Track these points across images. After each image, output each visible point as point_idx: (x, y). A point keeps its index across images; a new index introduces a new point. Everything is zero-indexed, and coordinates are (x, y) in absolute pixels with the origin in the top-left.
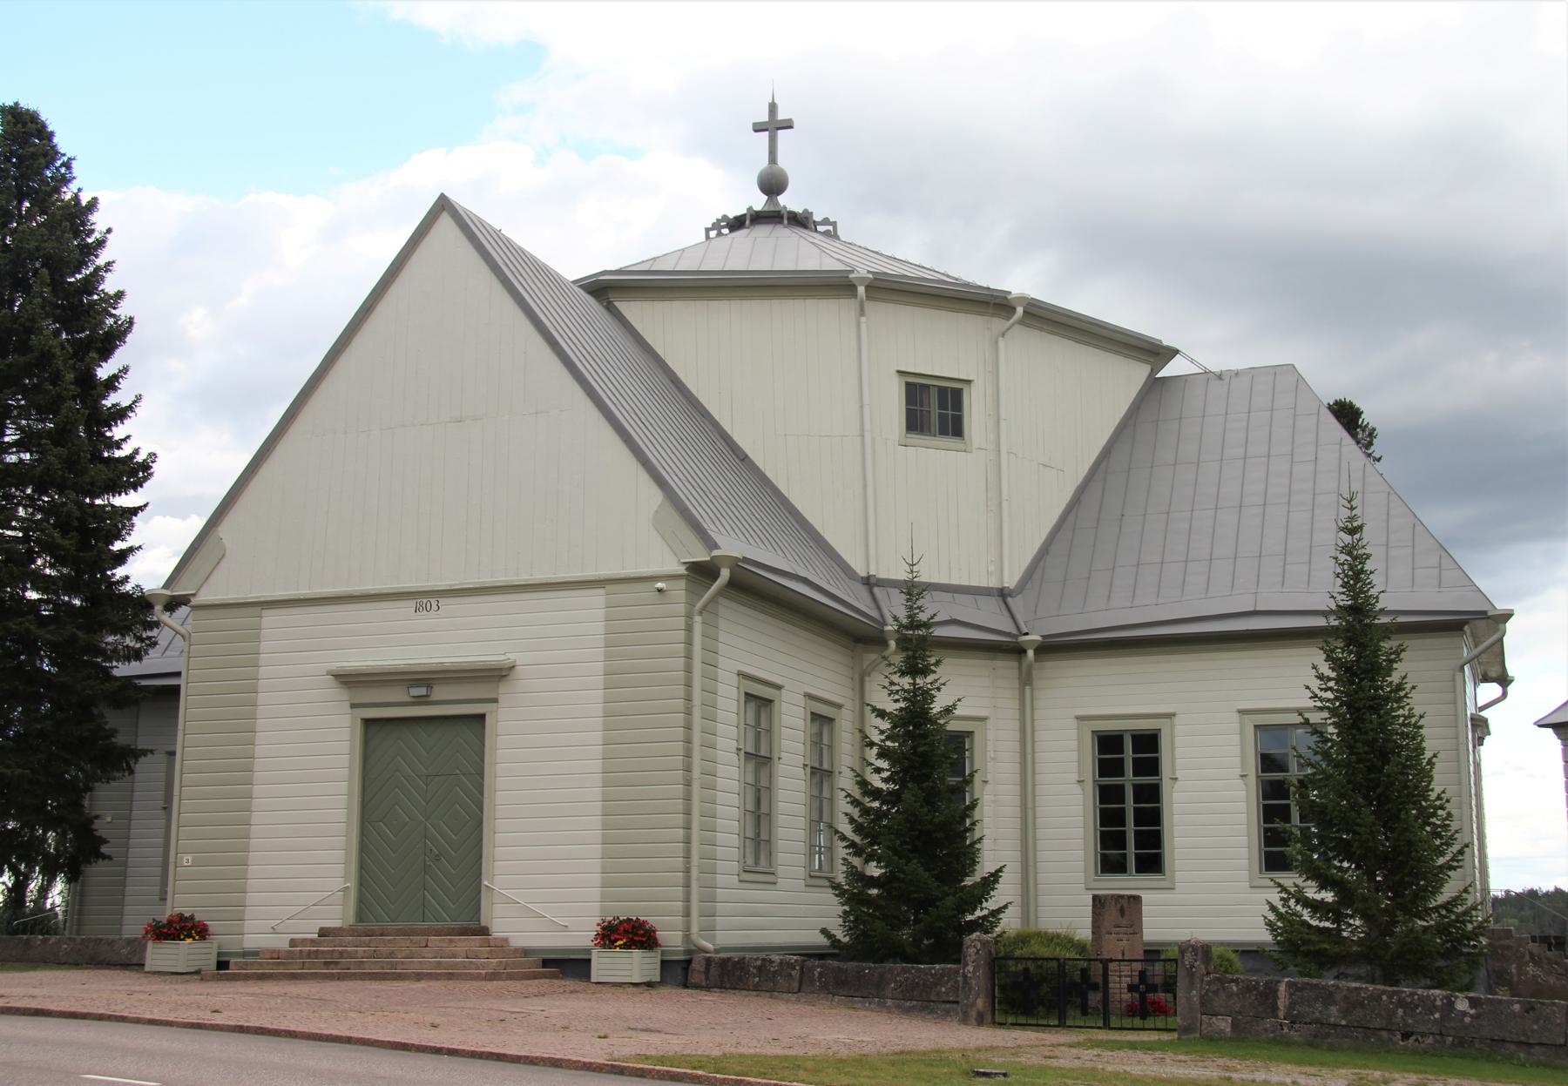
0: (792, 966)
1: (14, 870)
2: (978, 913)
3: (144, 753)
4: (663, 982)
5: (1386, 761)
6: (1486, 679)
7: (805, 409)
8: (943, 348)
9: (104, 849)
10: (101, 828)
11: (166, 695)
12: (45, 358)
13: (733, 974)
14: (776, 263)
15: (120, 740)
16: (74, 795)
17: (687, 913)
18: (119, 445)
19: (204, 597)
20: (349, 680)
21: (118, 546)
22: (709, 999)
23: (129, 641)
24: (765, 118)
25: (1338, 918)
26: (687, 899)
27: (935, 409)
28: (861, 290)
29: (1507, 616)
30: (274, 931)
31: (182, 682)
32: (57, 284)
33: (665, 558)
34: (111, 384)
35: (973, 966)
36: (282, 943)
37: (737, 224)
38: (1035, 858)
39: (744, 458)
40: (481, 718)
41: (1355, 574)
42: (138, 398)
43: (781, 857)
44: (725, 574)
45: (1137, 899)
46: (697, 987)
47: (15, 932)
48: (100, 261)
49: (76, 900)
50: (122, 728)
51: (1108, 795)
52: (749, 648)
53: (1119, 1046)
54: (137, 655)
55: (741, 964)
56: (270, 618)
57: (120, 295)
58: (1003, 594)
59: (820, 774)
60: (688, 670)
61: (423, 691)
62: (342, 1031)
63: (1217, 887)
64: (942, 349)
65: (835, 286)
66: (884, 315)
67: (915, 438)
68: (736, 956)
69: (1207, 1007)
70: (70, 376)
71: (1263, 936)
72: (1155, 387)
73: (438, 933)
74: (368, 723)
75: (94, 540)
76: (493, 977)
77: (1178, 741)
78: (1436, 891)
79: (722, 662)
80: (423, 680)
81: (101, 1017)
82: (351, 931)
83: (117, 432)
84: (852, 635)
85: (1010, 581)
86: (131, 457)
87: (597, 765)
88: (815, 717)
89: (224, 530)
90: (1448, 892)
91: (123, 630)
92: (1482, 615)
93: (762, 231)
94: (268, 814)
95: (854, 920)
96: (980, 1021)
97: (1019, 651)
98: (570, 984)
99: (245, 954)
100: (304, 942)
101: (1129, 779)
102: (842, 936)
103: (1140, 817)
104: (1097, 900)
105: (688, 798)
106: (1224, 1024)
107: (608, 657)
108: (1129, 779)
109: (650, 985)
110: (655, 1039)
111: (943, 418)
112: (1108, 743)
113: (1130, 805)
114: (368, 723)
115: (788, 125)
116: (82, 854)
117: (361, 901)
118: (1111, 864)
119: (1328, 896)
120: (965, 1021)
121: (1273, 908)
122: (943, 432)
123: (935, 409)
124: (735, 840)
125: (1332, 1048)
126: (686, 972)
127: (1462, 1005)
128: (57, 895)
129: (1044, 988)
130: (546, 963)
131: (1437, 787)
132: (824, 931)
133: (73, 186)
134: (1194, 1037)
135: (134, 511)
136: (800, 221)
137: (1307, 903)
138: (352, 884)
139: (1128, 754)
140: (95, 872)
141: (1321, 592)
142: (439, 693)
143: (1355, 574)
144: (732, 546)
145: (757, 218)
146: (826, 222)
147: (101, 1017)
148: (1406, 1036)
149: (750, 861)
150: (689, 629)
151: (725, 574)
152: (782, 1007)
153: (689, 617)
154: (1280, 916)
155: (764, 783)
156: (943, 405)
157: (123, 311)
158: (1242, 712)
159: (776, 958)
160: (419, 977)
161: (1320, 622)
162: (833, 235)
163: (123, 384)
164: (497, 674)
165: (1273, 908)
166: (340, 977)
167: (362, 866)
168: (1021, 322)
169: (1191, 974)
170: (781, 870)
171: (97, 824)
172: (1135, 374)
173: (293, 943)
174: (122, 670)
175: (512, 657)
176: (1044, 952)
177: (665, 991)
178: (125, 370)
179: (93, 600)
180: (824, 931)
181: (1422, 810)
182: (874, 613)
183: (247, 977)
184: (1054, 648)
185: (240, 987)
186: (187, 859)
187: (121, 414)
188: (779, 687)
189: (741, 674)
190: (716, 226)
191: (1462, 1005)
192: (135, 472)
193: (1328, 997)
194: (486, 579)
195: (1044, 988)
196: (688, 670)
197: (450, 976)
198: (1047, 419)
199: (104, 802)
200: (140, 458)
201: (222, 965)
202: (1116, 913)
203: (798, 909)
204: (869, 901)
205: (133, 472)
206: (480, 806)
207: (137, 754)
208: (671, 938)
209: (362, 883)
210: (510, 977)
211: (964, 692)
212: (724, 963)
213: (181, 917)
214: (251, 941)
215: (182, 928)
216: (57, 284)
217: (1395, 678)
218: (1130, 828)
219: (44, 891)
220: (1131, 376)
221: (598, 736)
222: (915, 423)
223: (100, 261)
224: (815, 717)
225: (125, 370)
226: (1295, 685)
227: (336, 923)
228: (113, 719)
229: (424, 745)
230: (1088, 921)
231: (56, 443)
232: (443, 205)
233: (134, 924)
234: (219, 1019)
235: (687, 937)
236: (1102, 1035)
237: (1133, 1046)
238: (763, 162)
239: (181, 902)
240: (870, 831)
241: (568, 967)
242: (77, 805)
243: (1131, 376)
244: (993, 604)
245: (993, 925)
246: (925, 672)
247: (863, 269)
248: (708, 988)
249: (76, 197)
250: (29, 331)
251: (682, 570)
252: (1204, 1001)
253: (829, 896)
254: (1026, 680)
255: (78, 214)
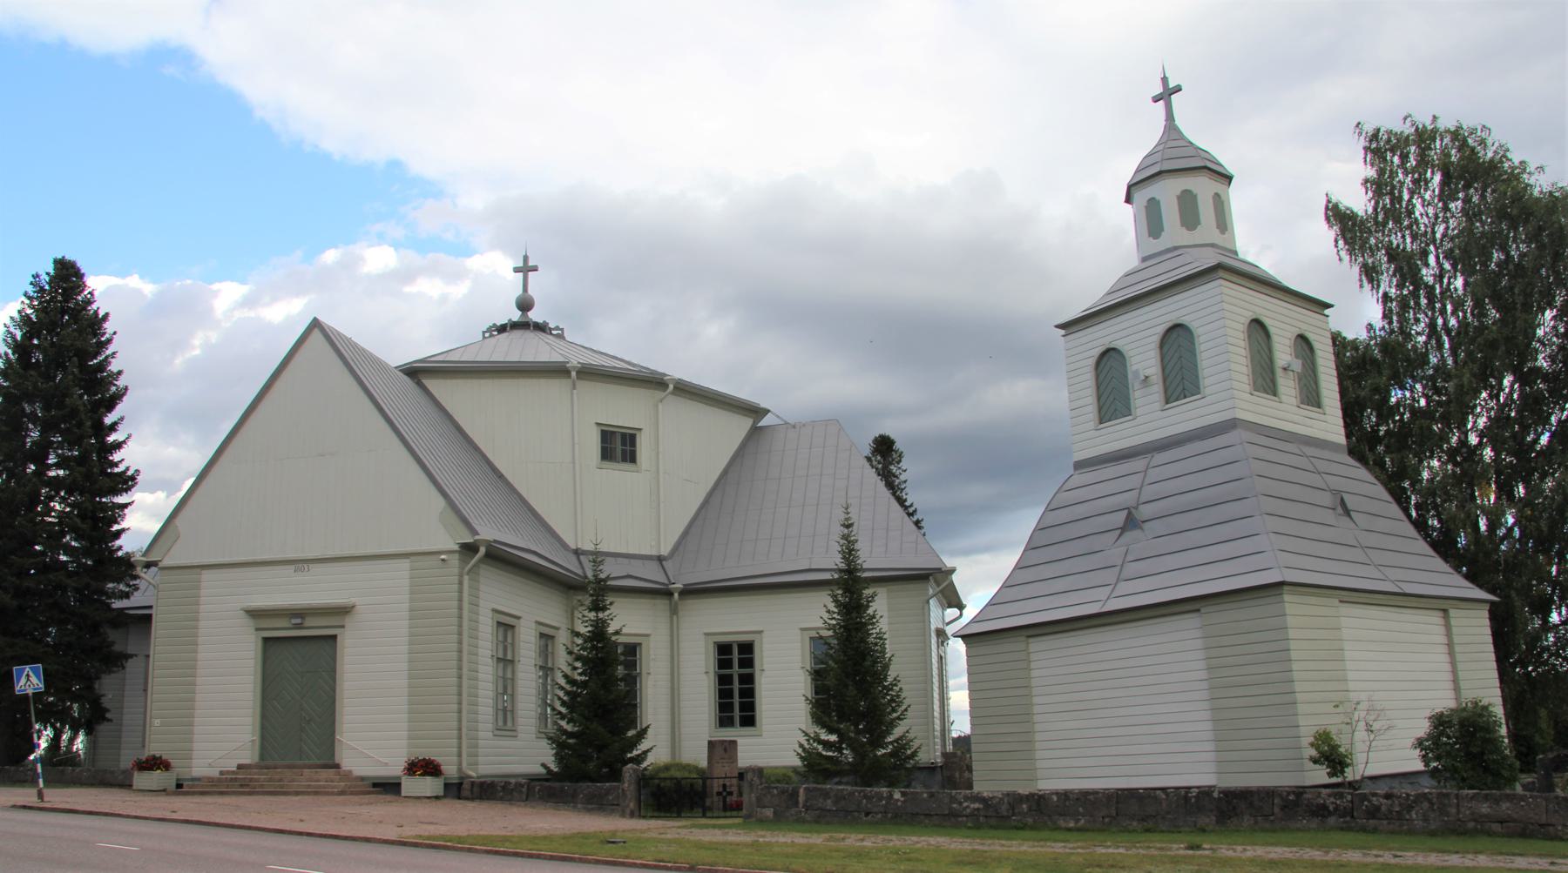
0: (522, 785)
1: (54, 728)
2: (635, 753)
3: (131, 656)
4: (445, 796)
5: (864, 660)
6: (950, 606)
7: (540, 444)
8: (624, 409)
9: (108, 715)
10: (106, 702)
11: (143, 620)
12: (74, 412)
13: (487, 791)
14: (522, 354)
15: (117, 648)
16: (89, 681)
17: (460, 755)
18: (116, 465)
19: (166, 562)
20: (255, 614)
21: (116, 527)
22: (470, 805)
23: (122, 587)
24: (521, 264)
25: (840, 750)
26: (460, 747)
27: (619, 446)
28: (574, 374)
29: (953, 571)
30: (210, 766)
31: (153, 612)
32: (83, 366)
33: (447, 540)
34: (113, 428)
35: (628, 783)
36: (214, 773)
37: (502, 329)
38: (675, 720)
39: (501, 476)
40: (334, 637)
41: (849, 552)
42: (129, 436)
43: (520, 721)
44: (483, 550)
45: (735, 742)
46: (467, 799)
47: (55, 765)
48: (109, 352)
49: (92, 746)
50: (119, 640)
51: (723, 680)
52: (499, 594)
53: (707, 826)
54: (127, 596)
55: (492, 785)
56: (207, 575)
57: (120, 373)
58: (660, 559)
59: (546, 670)
60: (460, 608)
61: (298, 621)
62: (246, 823)
63: (783, 731)
64: (625, 407)
65: (557, 371)
66: (588, 389)
67: (607, 464)
68: (489, 780)
69: (760, 803)
70: (89, 423)
71: (797, 762)
72: (755, 431)
73: (310, 767)
74: (266, 640)
75: (99, 523)
76: (342, 793)
77: (765, 646)
78: (889, 733)
79: (482, 603)
80: (300, 614)
81: (106, 814)
82: (257, 766)
83: (116, 457)
84: (564, 585)
85: (665, 551)
86: (124, 472)
87: (405, 666)
88: (542, 635)
89: (178, 521)
90: (897, 732)
91: (118, 580)
92: (939, 570)
93: (517, 334)
94: (205, 695)
95: (559, 758)
96: (632, 815)
97: (669, 594)
98: (388, 797)
99: (193, 779)
100: (228, 772)
101: (736, 670)
102: (554, 767)
103: (743, 693)
104: (711, 743)
105: (460, 686)
106: (769, 812)
107: (411, 600)
108: (736, 670)
109: (437, 798)
110: (431, 828)
111: (624, 452)
112: (723, 649)
113: (736, 686)
114: (266, 640)
115: (535, 269)
116: (94, 718)
117: (263, 747)
118: (725, 721)
119: (833, 738)
120: (623, 816)
121: (801, 746)
122: (624, 460)
123: (619, 446)
124: (491, 710)
125: (828, 823)
126: (457, 790)
127: (897, 796)
128: (80, 744)
129: (676, 795)
130: (375, 785)
131: (892, 674)
132: (543, 765)
133: (94, 306)
134: (753, 820)
135: (125, 506)
136: (541, 328)
137: (820, 742)
138: (257, 738)
139: (736, 656)
140: (103, 728)
141: (830, 560)
142: (309, 622)
143: (849, 552)
144: (487, 532)
145: (515, 326)
146: (557, 328)
147: (106, 814)
148: (867, 814)
149: (501, 723)
150: (461, 583)
151: (483, 550)
152: (515, 809)
153: (461, 576)
154: (804, 749)
155: (509, 675)
156: (624, 444)
157: (121, 382)
158: (803, 629)
159: (513, 781)
160: (297, 793)
161: (827, 576)
162: (561, 337)
163: (120, 427)
164: (344, 611)
165: (801, 746)
166: (250, 794)
167: (263, 728)
168: (672, 393)
169: (751, 785)
170: (519, 728)
171: (103, 700)
172: (745, 423)
173: (221, 773)
174: (118, 604)
175: (353, 600)
176: (678, 775)
177: (445, 801)
178: (122, 419)
179: (99, 562)
180: (543, 765)
181: (885, 687)
182: (579, 572)
183: (193, 793)
184: (691, 592)
185: (189, 799)
186: (157, 722)
187: (118, 446)
188: (518, 618)
189: (495, 611)
190: (489, 330)
191: (897, 796)
192: (126, 482)
193: (826, 795)
194: (338, 553)
195: (676, 795)
196: (460, 608)
197: (316, 793)
198: (686, 452)
199: (107, 686)
200: (130, 473)
201: (179, 786)
202: (722, 750)
203: (530, 753)
204: (568, 746)
205: (126, 482)
206: (334, 691)
207: (128, 657)
208: (450, 770)
209: (263, 738)
210: (352, 793)
211: (628, 620)
212: (482, 784)
213: (154, 758)
214: (198, 771)
215: (154, 764)
216: (83, 366)
217: (870, 611)
218: (736, 700)
219: (72, 740)
220: (743, 424)
221: (405, 648)
222: (607, 454)
223: (109, 352)
224: (542, 635)
225: (122, 419)
226: (818, 612)
227: (247, 761)
228: (112, 635)
229: (300, 656)
230: (705, 755)
231: (79, 464)
232: (316, 324)
233: (126, 762)
234: (174, 816)
235: (460, 770)
236: (704, 821)
237: (714, 826)
238: (520, 291)
239: (154, 749)
240: (572, 703)
241: (389, 787)
242: (90, 688)
243: (743, 424)
244: (654, 565)
245: (644, 759)
246: (604, 609)
247: (575, 359)
248: (472, 799)
249: (96, 312)
250: (65, 395)
251: (456, 548)
252: (759, 799)
253: (544, 743)
254: (674, 611)
255: (97, 323)
